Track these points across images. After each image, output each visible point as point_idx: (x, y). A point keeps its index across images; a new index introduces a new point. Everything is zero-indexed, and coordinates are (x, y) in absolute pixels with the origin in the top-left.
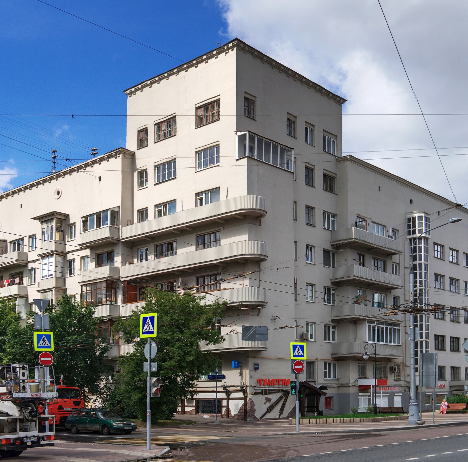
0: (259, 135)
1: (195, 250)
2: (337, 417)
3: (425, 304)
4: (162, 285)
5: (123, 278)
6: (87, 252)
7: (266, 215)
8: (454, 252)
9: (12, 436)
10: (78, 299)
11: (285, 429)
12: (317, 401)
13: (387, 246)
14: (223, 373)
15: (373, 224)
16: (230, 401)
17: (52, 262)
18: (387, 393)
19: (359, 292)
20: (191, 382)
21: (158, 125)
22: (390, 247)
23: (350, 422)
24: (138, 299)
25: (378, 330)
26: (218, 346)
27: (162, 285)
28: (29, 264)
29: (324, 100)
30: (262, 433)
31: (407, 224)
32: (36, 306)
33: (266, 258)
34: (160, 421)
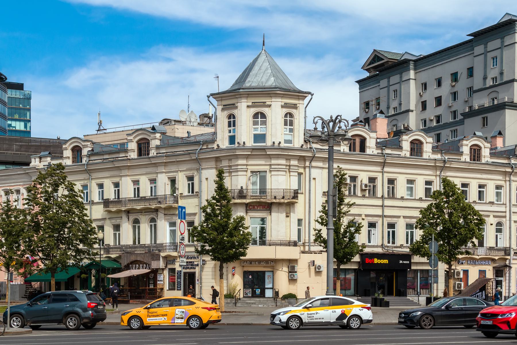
1: (375, 134)
2: (15, 285)
4: (101, 186)
6: (115, 305)
9: (258, 241)
10: (250, 187)
12: (208, 168)
16: (385, 214)
18: (513, 334)
19: (497, 43)
20: (199, 229)
22: (443, 66)
25: (335, 289)
26: (152, 216)
27: (101, 186)
29: (250, 326)
31: (396, 230)
32: (118, 255)
33: (362, 90)
34: (386, 261)
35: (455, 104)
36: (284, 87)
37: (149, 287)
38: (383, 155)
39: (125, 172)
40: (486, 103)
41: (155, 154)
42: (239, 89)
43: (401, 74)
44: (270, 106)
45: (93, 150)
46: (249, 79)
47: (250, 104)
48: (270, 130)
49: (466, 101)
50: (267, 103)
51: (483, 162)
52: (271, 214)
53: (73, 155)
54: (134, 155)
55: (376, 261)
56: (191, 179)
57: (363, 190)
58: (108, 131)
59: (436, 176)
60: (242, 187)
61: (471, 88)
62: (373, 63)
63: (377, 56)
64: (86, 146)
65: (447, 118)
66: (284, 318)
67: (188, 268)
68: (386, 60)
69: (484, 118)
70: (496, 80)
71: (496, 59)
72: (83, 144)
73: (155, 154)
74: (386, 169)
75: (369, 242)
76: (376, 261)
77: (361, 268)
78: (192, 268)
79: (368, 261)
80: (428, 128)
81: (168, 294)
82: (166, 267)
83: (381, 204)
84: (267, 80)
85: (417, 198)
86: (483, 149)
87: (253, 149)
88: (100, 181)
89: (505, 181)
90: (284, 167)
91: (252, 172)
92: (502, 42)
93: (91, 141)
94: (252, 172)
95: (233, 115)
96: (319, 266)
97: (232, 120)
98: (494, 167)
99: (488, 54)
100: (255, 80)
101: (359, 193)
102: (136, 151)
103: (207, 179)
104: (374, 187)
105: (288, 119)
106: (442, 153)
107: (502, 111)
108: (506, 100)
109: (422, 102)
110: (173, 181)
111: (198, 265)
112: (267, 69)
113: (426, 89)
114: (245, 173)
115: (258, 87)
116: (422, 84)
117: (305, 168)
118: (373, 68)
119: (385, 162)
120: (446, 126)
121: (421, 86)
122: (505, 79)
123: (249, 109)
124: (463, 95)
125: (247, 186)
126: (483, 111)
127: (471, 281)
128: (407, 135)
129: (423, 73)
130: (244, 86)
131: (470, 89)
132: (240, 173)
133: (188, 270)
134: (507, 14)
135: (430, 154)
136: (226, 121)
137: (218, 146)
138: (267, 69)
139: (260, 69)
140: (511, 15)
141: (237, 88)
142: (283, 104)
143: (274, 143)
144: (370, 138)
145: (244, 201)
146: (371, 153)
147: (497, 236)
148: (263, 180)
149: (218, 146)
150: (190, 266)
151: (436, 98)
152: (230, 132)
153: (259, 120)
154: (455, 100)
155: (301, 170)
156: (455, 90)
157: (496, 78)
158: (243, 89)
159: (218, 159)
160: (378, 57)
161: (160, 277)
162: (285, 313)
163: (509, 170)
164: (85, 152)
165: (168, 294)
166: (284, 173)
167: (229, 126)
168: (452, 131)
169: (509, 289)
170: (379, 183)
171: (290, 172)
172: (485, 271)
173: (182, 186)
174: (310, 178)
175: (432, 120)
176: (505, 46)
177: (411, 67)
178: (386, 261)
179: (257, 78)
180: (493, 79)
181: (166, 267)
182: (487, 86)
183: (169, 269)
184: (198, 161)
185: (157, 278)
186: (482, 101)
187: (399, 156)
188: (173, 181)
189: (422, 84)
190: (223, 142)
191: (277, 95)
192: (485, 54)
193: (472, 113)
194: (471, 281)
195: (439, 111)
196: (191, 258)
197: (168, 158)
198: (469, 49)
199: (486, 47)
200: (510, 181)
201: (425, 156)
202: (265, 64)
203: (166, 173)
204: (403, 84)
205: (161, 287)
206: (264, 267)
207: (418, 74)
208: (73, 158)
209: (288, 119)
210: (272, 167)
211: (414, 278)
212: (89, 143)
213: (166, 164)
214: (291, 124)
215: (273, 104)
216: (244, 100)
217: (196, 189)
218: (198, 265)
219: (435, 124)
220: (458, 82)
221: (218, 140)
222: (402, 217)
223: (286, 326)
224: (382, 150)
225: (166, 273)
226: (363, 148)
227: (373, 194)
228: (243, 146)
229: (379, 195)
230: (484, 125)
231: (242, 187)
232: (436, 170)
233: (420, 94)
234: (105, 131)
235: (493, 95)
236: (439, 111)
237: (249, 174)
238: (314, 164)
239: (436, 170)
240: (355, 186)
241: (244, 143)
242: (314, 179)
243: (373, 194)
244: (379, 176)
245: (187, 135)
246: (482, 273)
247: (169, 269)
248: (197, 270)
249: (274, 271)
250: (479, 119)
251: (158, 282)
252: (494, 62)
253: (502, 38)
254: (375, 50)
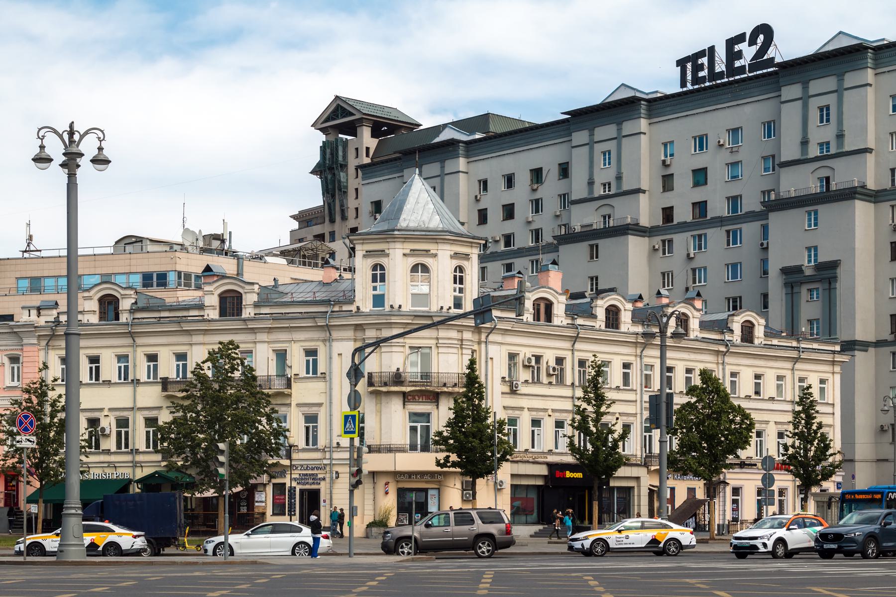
4: (152, 358)
27: (152, 358)
35: (537, 218)
36: (453, 230)
37: (239, 510)
38: (574, 326)
39: (197, 339)
40: (597, 222)
41: (252, 315)
42: (393, 230)
43: (443, 162)
44: (435, 255)
45: (136, 303)
46: (403, 217)
47: (408, 251)
48: (435, 289)
49: (557, 216)
50: (432, 252)
51: (692, 337)
52: (438, 408)
53: (100, 308)
54: (214, 314)
55: (569, 474)
56: (311, 353)
57: (549, 375)
58: (43, 254)
59: (636, 356)
60: (398, 369)
61: (564, 195)
62: (334, 119)
63: (342, 107)
64: (125, 296)
65: (524, 240)
66: (587, 544)
67: (308, 483)
68: (358, 116)
69: (591, 246)
70: (609, 188)
71: (609, 154)
72: (123, 292)
73: (252, 315)
74: (578, 346)
75: (556, 448)
76: (569, 474)
77: (549, 484)
78: (313, 483)
79: (558, 474)
80: (491, 253)
81: (271, 519)
82: (270, 481)
83: (571, 395)
84: (430, 220)
85: (614, 386)
86: (691, 320)
87: (416, 316)
88: (151, 350)
89: (718, 363)
90: (456, 342)
91: (411, 347)
92: (619, 130)
93: (135, 289)
94: (411, 347)
95: (381, 265)
96: (501, 482)
97: (378, 272)
98: (705, 344)
99: (595, 145)
100: (413, 218)
101: (544, 379)
102: (218, 308)
103: (340, 355)
104: (562, 370)
105: (458, 274)
106: (643, 325)
107: (622, 238)
108: (629, 221)
109: (479, 211)
110: (281, 355)
111: (324, 479)
112: (427, 203)
113: (485, 189)
114: (401, 349)
115: (419, 228)
116: (480, 181)
117: (479, 343)
118: (331, 127)
119: (577, 337)
120: (522, 252)
121: (477, 184)
122: (626, 187)
123: (405, 258)
124: (551, 205)
125: (405, 369)
126: (589, 235)
127: (678, 503)
128: (602, 299)
129: (480, 164)
130: (399, 227)
131: (563, 197)
132: (394, 349)
133: (307, 487)
134: (623, 84)
135: (629, 326)
136: (370, 273)
137: (358, 308)
138: (427, 203)
139: (417, 202)
140: (634, 89)
141: (386, 228)
142: (452, 253)
143: (442, 308)
144: (558, 302)
145: (403, 389)
146: (560, 324)
147: (533, 432)
148: (426, 360)
149: (358, 308)
150: (311, 481)
151: (503, 206)
152: (375, 288)
153: (420, 274)
154: (537, 211)
155: (476, 347)
156: (537, 196)
157: (609, 184)
158: (399, 230)
159: (358, 327)
160: (344, 109)
161: (259, 497)
162: (586, 538)
163: (723, 349)
164: (125, 304)
165: (271, 519)
166: (455, 351)
167: (374, 279)
168: (533, 262)
169: (724, 515)
170: (568, 365)
171: (462, 348)
172: (695, 489)
173: (297, 362)
174: (487, 358)
175: (497, 242)
176: (624, 136)
177: (461, 152)
178: (579, 475)
179: (415, 215)
180: (605, 185)
181: (270, 481)
182: (596, 195)
183: (274, 484)
184: (328, 328)
185: (254, 497)
186: (584, 217)
187: (592, 328)
188: (281, 355)
189: (480, 181)
190: (364, 301)
191: (445, 241)
192: (591, 144)
193: (569, 238)
194: (678, 503)
195: (509, 227)
196: (313, 469)
197: (276, 322)
198: (562, 133)
199: (592, 135)
200: (723, 363)
201: (623, 328)
202: (422, 195)
203: (268, 342)
204: (447, 178)
205: (261, 511)
206: (427, 482)
207: (472, 165)
208: (100, 313)
209: (458, 274)
210: (440, 341)
211: (609, 499)
212: (132, 292)
213: (270, 330)
214: (461, 282)
215: (440, 253)
216: (398, 245)
217: (321, 368)
218: (324, 479)
219: (502, 247)
220: (542, 183)
221: (356, 299)
222: (526, 410)
223: (588, 553)
224: (573, 319)
225: (270, 489)
226: (549, 318)
227: (561, 381)
228: (397, 311)
229: (569, 381)
230: (592, 258)
231: (398, 369)
232: (636, 347)
233: (476, 197)
234: (38, 254)
235: (606, 211)
236: (509, 227)
237: (408, 351)
238: (492, 338)
239: (636, 347)
240: (538, 368)
241: (400, 307)
242: (491, 359)
243: (561, 381)
244: (567, 355)
245: (273, 284)
246: (691, 491)
247: (274, 484)
248: (323, 487)
249: (442, 489)
250: (583, 248)
251: (256, 504)
252: (605, 159)
253: (619, 124)
254: (337, 97)
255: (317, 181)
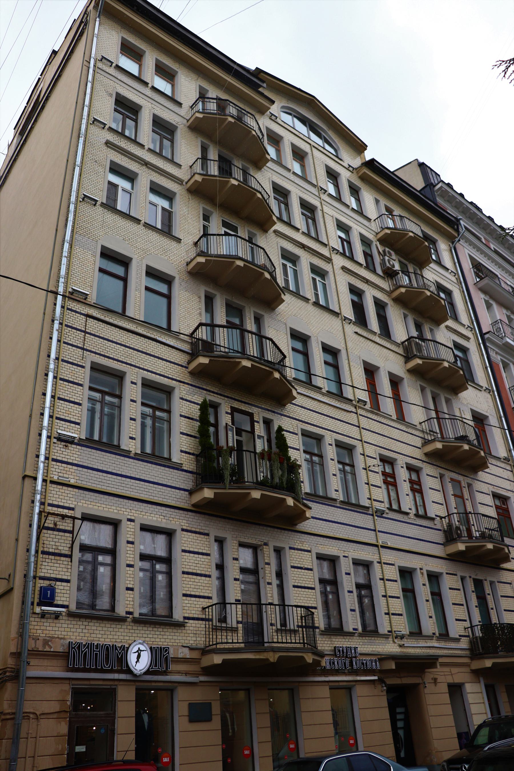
0: (169, 467)
3: (56, 293)
5: (17, 649)
7: (113, 106)
8: (254, 336)
11: (44, 103)
13: (142, 119)
14: (433, 288)
15: (148, 536)
17: (447, 327)
21: (204, 219)
23: (41, 528)
24: (404, 593)
28: (200, 403)
30: (331, 135)
34: (230, 734)
46: (57, 598)
255: (249, 61)
